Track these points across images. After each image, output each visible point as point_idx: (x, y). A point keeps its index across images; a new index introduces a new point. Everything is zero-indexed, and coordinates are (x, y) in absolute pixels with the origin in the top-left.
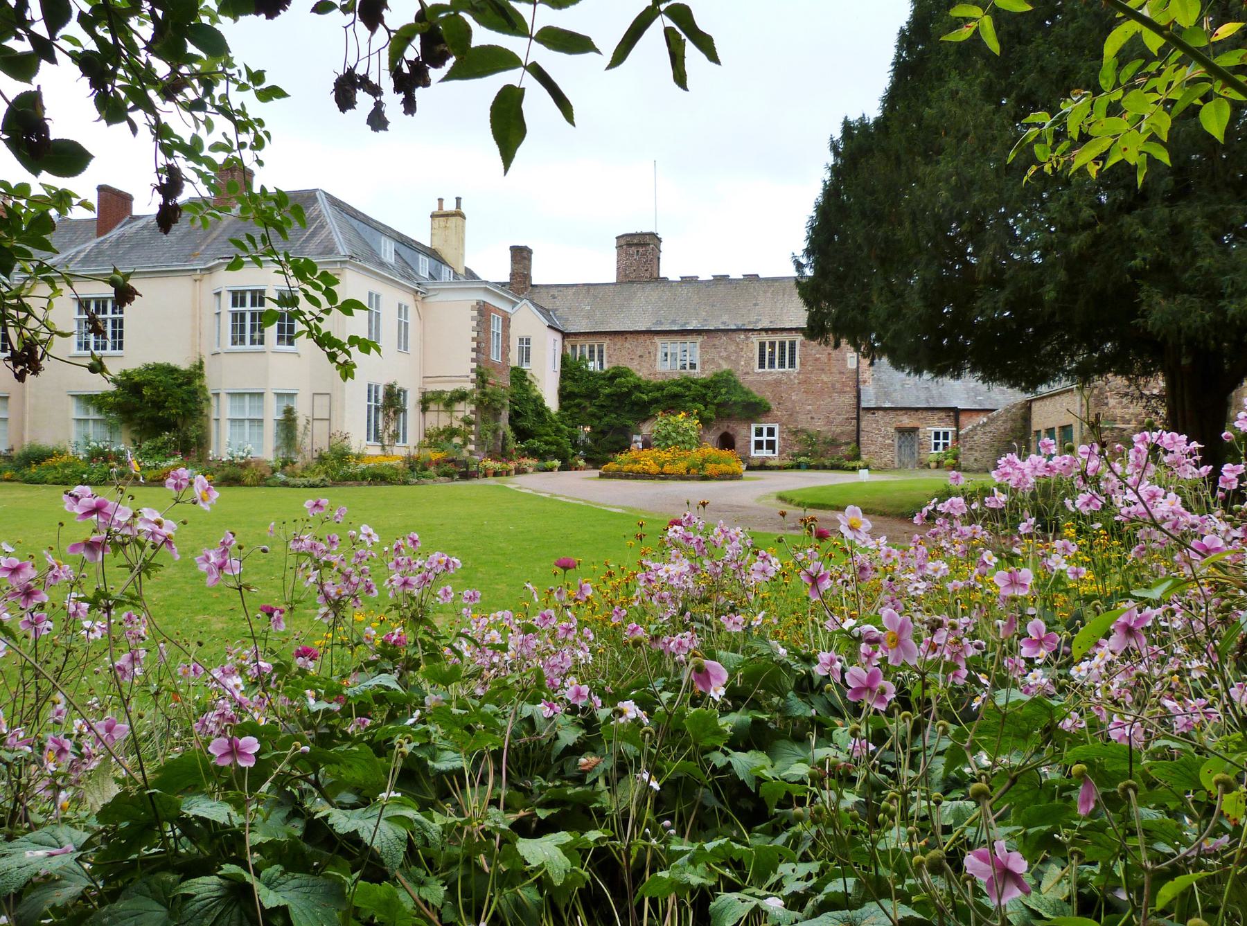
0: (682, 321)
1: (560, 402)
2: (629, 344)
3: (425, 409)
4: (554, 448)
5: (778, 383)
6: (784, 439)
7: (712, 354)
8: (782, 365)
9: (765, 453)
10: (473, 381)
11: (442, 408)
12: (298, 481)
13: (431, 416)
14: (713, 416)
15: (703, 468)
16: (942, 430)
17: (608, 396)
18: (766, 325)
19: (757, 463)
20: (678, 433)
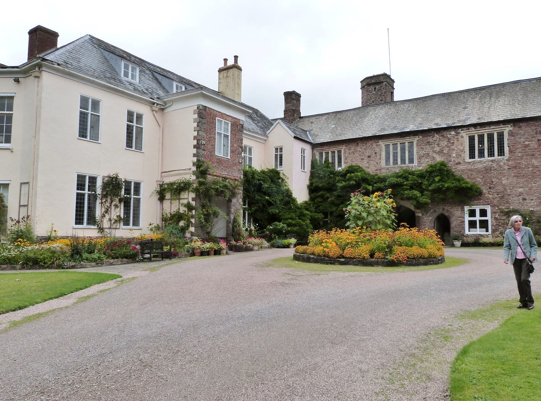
1: (310, 194)
2: (360, 148)
3: (162, 198)
5: (488, 170)
6: (496, 219)
8: (491, 154)
9: (478, 231)
13: (166, 203)
14: (429, 201)
15: (391, 252)
18: (474, 121)
19: (470, 240)
20: (369, 213)
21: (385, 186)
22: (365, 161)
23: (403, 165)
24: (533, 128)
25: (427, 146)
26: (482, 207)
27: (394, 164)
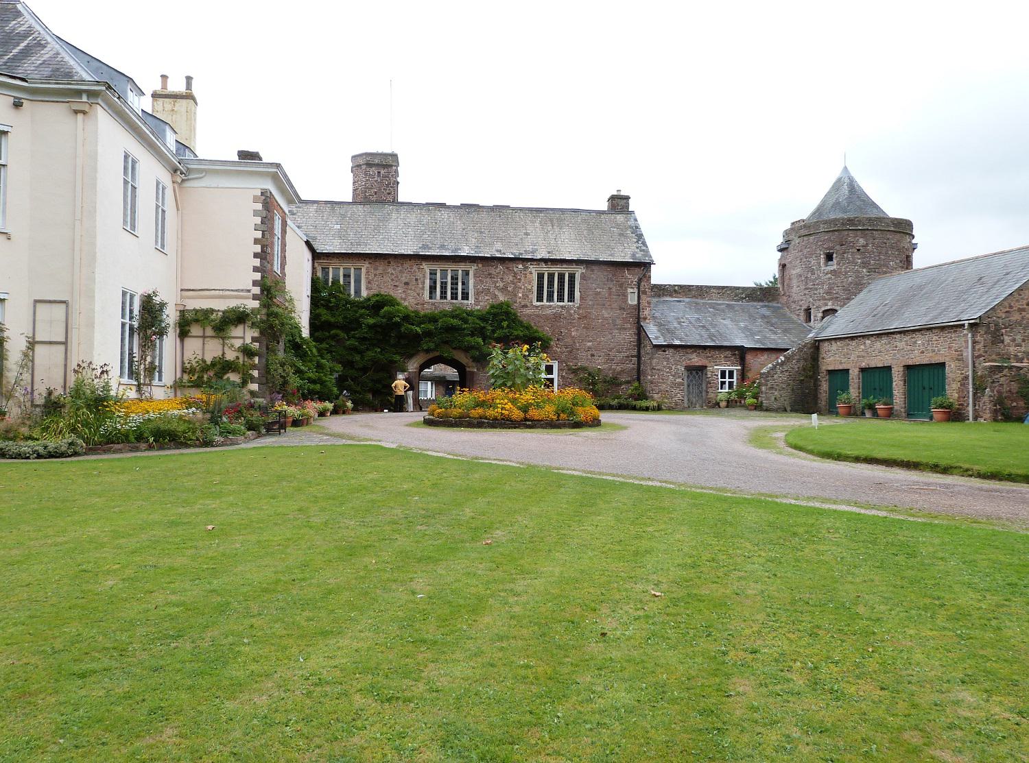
0: (452, 246)
3: (183, 334)
4: (318, 387)
5: (557, 317)
7: (488, 283)
8: (561, 299)
10: (255, 297)
11: (209, 332)
12: (26, 447)
16: (727, 368)
17: (371, 327)
21: (436, 329)
23: (454, 301)
24: (606, 274)
25: (488, 279)
27: (441, 298)
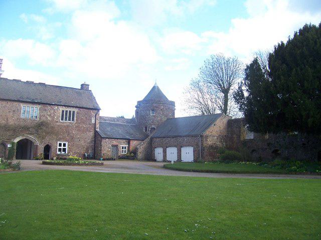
5: (68, 126)
22: (11, 114)
26: (65, 142)
